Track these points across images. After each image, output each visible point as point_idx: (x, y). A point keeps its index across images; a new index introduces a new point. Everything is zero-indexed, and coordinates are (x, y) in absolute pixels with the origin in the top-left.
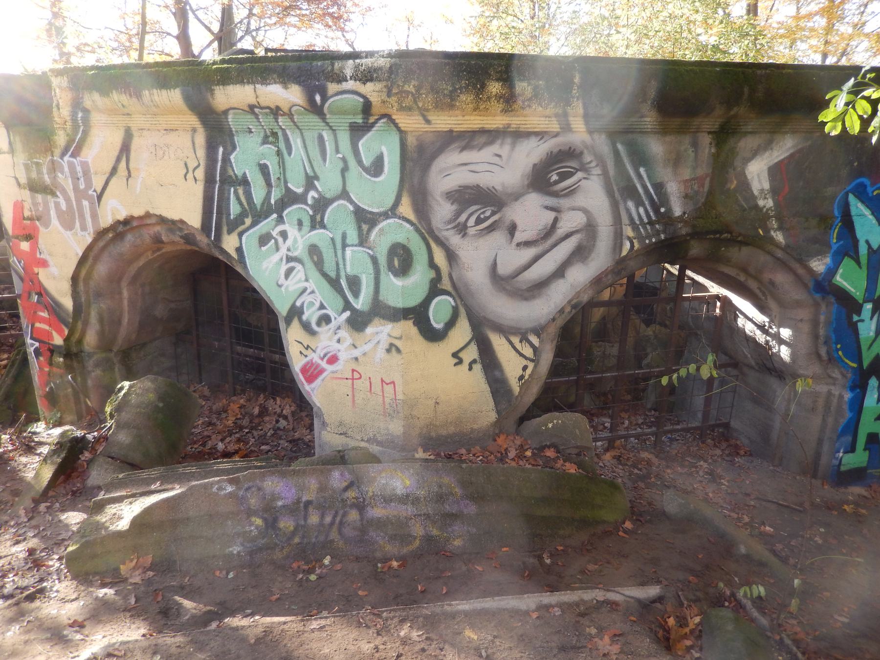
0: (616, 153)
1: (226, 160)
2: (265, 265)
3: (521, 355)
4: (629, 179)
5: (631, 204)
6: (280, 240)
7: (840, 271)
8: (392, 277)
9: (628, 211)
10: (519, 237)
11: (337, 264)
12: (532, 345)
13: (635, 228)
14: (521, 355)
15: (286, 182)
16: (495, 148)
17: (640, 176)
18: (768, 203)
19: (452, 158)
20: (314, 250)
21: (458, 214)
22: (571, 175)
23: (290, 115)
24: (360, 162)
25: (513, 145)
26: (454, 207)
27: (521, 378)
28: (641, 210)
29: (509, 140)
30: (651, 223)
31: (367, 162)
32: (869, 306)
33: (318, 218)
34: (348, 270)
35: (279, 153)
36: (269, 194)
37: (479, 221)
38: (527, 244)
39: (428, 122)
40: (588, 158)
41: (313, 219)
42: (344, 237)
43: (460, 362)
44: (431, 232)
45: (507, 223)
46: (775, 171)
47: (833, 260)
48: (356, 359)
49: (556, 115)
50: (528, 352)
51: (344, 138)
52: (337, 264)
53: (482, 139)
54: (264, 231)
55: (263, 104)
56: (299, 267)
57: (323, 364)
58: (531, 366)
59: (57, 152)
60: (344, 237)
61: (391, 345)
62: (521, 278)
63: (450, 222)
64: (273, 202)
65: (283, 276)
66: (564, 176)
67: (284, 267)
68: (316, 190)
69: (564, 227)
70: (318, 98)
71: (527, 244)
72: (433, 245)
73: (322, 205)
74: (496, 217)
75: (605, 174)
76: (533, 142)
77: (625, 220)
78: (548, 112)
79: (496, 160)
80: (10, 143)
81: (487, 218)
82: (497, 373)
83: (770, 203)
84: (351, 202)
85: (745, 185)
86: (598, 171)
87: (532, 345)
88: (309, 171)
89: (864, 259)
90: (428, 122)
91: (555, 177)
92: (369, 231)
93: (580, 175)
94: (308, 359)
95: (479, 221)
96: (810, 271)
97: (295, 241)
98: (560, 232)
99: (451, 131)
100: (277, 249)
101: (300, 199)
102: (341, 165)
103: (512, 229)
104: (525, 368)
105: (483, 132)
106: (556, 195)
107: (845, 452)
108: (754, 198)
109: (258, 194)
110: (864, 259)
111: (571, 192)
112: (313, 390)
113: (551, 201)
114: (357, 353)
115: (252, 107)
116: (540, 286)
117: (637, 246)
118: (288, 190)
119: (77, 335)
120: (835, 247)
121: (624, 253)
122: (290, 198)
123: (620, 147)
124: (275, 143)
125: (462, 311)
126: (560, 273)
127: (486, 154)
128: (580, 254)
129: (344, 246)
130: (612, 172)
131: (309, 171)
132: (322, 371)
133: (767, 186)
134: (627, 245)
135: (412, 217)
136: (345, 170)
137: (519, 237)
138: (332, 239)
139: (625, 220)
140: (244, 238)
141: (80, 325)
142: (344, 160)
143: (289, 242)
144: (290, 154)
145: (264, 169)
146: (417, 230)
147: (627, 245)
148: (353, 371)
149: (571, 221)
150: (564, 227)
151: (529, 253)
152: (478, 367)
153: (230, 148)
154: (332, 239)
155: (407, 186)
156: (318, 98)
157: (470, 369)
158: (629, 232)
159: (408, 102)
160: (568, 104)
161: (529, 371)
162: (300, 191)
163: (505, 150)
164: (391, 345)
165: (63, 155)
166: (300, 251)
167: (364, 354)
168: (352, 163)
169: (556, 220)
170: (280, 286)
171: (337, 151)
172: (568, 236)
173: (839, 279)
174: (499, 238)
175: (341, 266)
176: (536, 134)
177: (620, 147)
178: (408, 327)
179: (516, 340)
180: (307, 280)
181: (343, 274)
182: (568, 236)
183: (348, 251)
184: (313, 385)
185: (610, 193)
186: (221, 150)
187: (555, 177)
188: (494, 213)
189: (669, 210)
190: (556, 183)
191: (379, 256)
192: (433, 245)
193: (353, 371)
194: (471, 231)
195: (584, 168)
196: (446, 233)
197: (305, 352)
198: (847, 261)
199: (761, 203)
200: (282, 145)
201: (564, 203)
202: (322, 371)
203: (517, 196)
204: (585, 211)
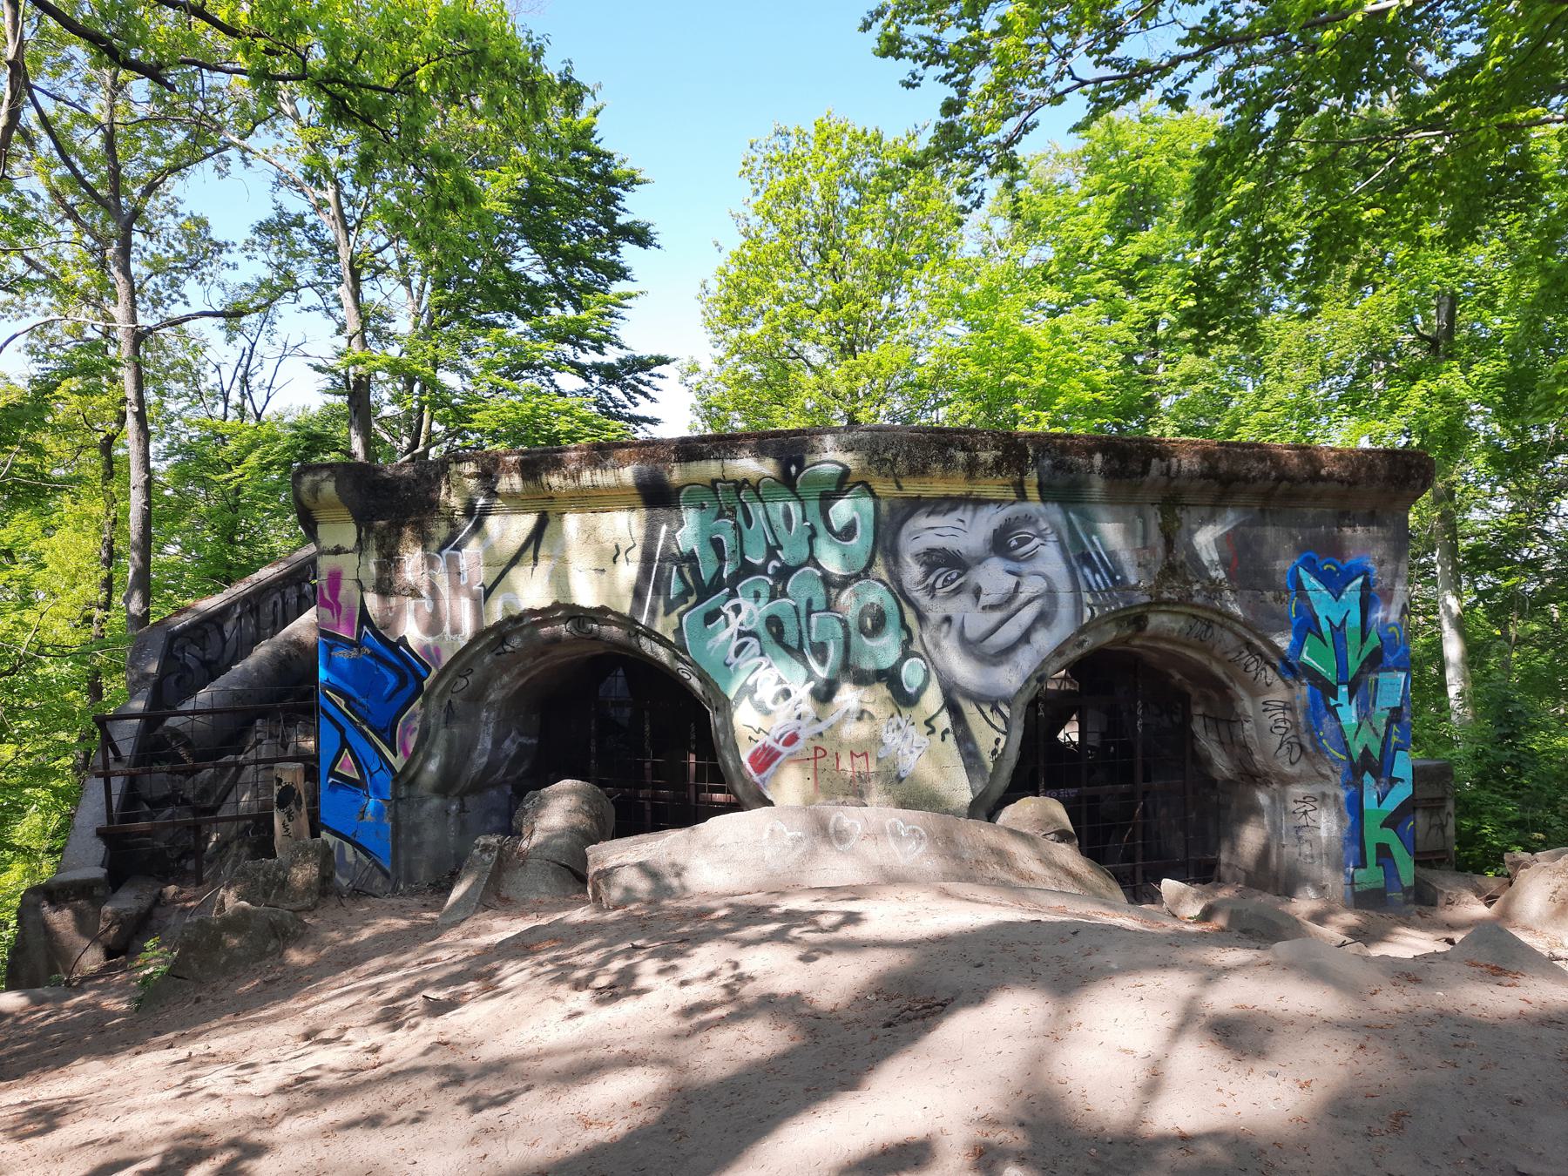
0: (1070, 523)
1: (671, 536)
2: (710, 644)
3: (993, 726)
4: (1084, 547)
5: (1087, 571)
6: (731, 615)
7: (1306, 649)
8: (867, 641)
9: (1085, 577)
10: (984, 600)
11: (800, 632)
12: (1003, 716)
13: (1094, 596)
14: (993, 726)
15: (743, 555)
16: (958, 514)
17: (1093, 544)
18: (1219, 574)
19: (921, 521)
20: (774, 623)
21: (927, 575)
22: (1028, 541)
23: (756, 489)
24: (829, 528)
25: (975, 511)
26: (923, 569)
27: (994, 752)
28: (1098, 577)
29: (970, 507)
30: (1108, 590)
31: (837, 527)
32: (1344, 689)
33: (780, 587)
34: (813, 637)
35: (736, 526)
36: (721, 569)
37: (946, 583)
38: (993, 607)
39: (900, 488)
40: (1043, 525)
41: (773, 590)
42: (809, 603)
43: (933, 731)
44: (902, 592)
45: (972, 585)
46: (1220, 543)
47: (1296, 635)
48: (821, 734)
49: (1014, 484)
50: (999, 723)
51: (813, 507)
52: (800, 632)
53: (946, 506)
54: (712, 608)
55: (729, 477)
56: (753, 641)
57: (779, 747)
58: (1003, 739)
59: (435, 545)
60: (809, 603)
61: (863, 712)
62: (986, 643)
63: (919, 583)
64: (725, 576)
65: (732, 654)
66: (1024, 542)
67: (735, 644)
68: (778, 558)
69: (1027, 591)
70: (793, 469)
71: (993, 607)
72: (904, 605)
73: (784, 573)
74: (961, 580)
75: (1060, 541)
76: (992, 509)
77: (1084, 587)
78: (1006, 481)
79: (960, 525)
80: (359, 539)
81: (953, 581)
82: (970, 746)
83: (1222, 575)
84: (818, 567)
85: (1194, 557)
86: (1053, 537)
87: (1003, 716)
88: (771, 540)
89: (1328, 636)
90: (900, 488)
91: (1014, 543)
92: (838, 594)
93: (1037, 541)
94: (759, 744)
95: (946, 583)
96: (1275, 649)
97: (751, 614)
98: (1022, 597)
99: (919, 497)
100: (727, 625)
101: (762, 570)
102: (809, 532)
103: (977, 592)
104: (997, 741)
105: (947, 498)
106: (1016, 559)
107: (1355, 867)
108: (1206, 569)
109: (707, 573)
110: (1328, 636)
111: (1030, 557)
112: (763, 781)
113: (1012, 566)
114: (821, 727)
115: (714, 482)
116: (1007, 652)
117: (1097, 613)
118: (745, 562)
119: (411, 773)
120: (1296, 622)
121: (1086, 621)
122: (747, 569)
123: (1072, 516)
124: (733, 516)
125: (933, 675)
126: (1025, 638)
127: (950, 520)
128: (1043, 619)
129: (809, 613)
130: (1067, 540)
131: (771, 540)
132: (778, 754)
133: (1216, 557)
134: (1088, 612)
135: (885, 577)
136: (813, 535)
137: (985, 600)
138: (795, 608)
139: (1084, 587)
140: (685, 618)
141: (421, 756)
142: (812, 527)
143: (743, 616)
144: (749, 526)
145: (717, 545)
146: (889, 590)
147: (1088, 612)
148: (816, 748)
149: (1031, 587)
150: (1027, 591)
151: (997, 616)
152: (950, 738)
153: (675, 525)
154: (795, 608)
155: (880, 547)
156: (793, 469)
157: (943, 739)
158: (1088, 598)
159: (886, 469)
160: (1023, 473)
161: (1002, 745)
162: (759, 561)
163: (967, 516)
164: (863, 712)
165: (443, 547)
166: (758, 625)
167: (831, 727)
168: (821, 527)
169: (1018, 584)
170: (728, 665)
171: (804, 520)
172: (1029, 601)
173: (1305, 657)
174: (965, 600)
175: (805, 634)
176: (995, 501)
177: (1072, 516)
178: (882, 690)
179: (987, 709)
180: (762, 654)
181: (806, 642)
182: (1029, 601)
183: (814, 618)
184: (764, 775)
185: (1067, 561)
186: (664, 528)
187: (1014, 543)
188: (959, 576)
189: (1124, 578)
190: (1016, 548)
191: (849, 618)
192: (904, 605)
193: (816, 748)
194: (940, 593)
195: (1040, 535)
196: (916, 594)
197: (755, 736)
198: (1310, 637)
199: (1213, 574)
200: (740, 518)
201: (1025, 568)
202: (778, 754)
203: (980, 561)
204: (1045, 576)
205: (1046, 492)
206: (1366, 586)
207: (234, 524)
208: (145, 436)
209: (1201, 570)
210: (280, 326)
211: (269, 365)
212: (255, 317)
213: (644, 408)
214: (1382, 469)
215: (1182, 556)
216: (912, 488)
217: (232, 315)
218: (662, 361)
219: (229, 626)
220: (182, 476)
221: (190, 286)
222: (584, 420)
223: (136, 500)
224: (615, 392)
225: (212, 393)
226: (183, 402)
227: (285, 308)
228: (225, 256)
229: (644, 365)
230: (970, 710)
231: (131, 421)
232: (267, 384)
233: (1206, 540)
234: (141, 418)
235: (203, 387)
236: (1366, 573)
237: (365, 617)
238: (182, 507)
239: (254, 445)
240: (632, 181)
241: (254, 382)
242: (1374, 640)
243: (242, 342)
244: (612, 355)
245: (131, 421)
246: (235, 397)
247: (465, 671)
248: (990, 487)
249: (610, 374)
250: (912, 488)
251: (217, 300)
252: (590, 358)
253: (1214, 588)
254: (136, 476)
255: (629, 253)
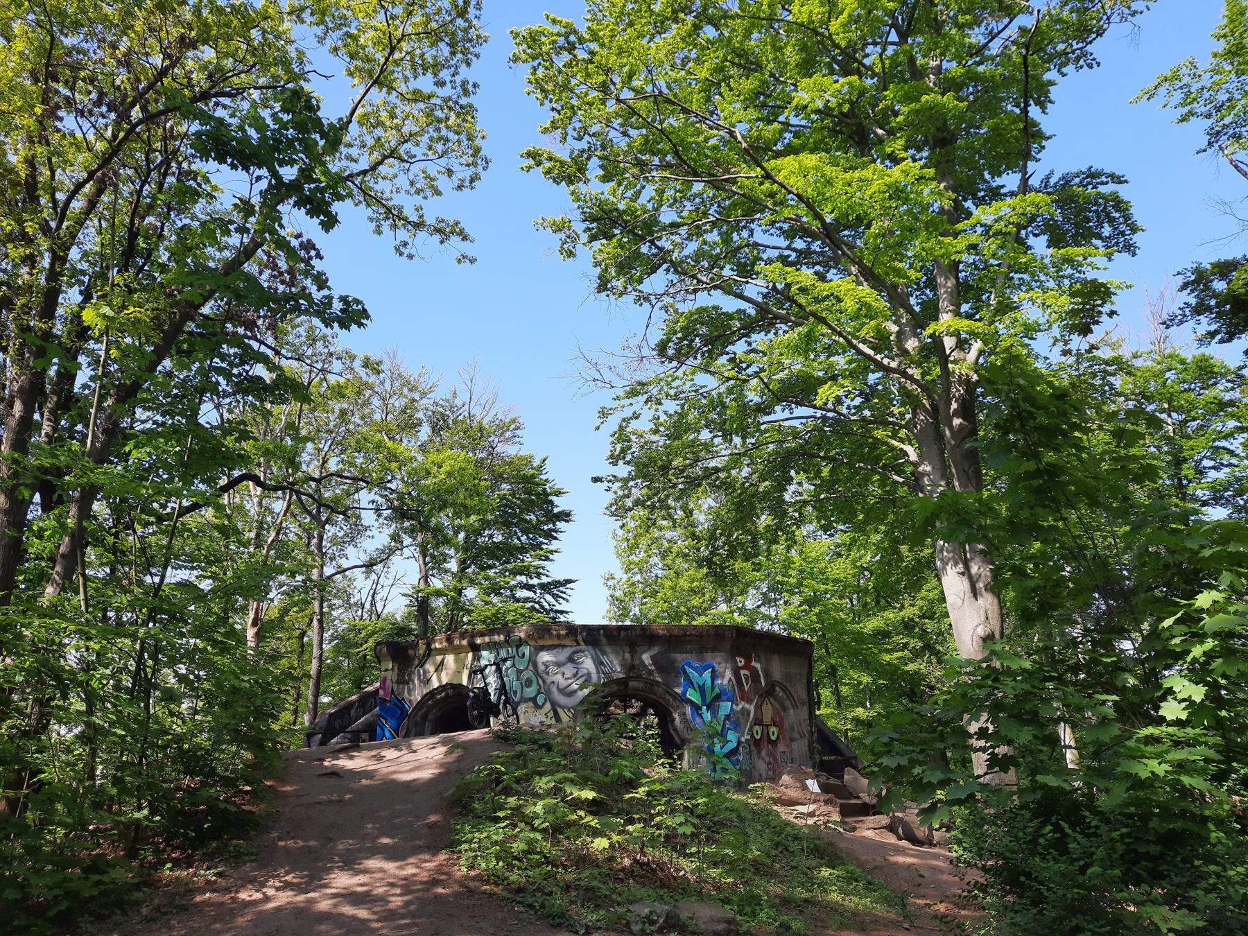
85: (642, 662)
178: (531, 704)
205: (586, 642)
206: (713, 672)
207: (362, 677)
208: (322, 630)
209: (645, 666)
210: (393, 569)
211: (386, 589)
212: (380, 565)
213: (563, 606)
214: (712, 632)
215: (637, 662)
216: (541, 643)
217: (369, 566)
218: (569, 581)
219: (353, 712)
220: (337, 650)
221: (350, 550)
222: (522, 615)
223: (315, 663)
224: (548, 597)
225: (356, 604)
226: (341, 611)
227: (396, 559)
228: (368, 533)
229: (558, 584)
230: (560, 711)
231: (315, 623)
232: (637, 340)
233: (646, 658)
234: (321, 622)
235: (352, 601)
236: (713, 667)
237: (393, 692)
238: (337, 667)
239: (373, 633)
240: (558, 493)
241: (378, 597)
242: (717, 690)
243: (374, 576)
244: (545, 580)
245: (315, 623)
246: (367, 606)
247: (420, 709)
248: (567, 642)
249: (545, 587)
250: (541, 643)
251: (364, 558)
252: (535, 581)
253: (651, 672)
254: (316, 652)
255: (560, 525)
